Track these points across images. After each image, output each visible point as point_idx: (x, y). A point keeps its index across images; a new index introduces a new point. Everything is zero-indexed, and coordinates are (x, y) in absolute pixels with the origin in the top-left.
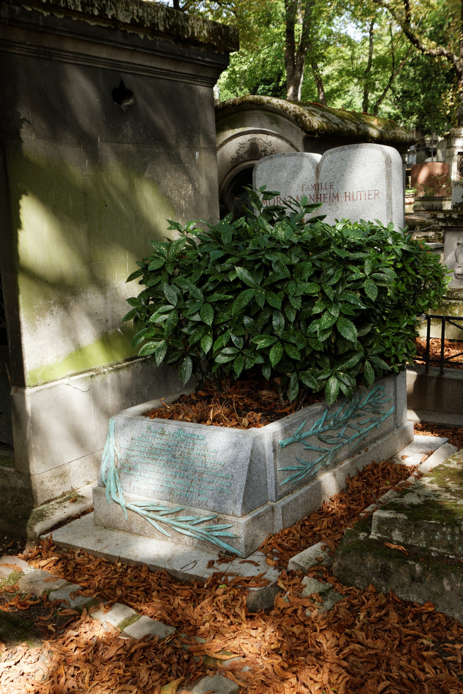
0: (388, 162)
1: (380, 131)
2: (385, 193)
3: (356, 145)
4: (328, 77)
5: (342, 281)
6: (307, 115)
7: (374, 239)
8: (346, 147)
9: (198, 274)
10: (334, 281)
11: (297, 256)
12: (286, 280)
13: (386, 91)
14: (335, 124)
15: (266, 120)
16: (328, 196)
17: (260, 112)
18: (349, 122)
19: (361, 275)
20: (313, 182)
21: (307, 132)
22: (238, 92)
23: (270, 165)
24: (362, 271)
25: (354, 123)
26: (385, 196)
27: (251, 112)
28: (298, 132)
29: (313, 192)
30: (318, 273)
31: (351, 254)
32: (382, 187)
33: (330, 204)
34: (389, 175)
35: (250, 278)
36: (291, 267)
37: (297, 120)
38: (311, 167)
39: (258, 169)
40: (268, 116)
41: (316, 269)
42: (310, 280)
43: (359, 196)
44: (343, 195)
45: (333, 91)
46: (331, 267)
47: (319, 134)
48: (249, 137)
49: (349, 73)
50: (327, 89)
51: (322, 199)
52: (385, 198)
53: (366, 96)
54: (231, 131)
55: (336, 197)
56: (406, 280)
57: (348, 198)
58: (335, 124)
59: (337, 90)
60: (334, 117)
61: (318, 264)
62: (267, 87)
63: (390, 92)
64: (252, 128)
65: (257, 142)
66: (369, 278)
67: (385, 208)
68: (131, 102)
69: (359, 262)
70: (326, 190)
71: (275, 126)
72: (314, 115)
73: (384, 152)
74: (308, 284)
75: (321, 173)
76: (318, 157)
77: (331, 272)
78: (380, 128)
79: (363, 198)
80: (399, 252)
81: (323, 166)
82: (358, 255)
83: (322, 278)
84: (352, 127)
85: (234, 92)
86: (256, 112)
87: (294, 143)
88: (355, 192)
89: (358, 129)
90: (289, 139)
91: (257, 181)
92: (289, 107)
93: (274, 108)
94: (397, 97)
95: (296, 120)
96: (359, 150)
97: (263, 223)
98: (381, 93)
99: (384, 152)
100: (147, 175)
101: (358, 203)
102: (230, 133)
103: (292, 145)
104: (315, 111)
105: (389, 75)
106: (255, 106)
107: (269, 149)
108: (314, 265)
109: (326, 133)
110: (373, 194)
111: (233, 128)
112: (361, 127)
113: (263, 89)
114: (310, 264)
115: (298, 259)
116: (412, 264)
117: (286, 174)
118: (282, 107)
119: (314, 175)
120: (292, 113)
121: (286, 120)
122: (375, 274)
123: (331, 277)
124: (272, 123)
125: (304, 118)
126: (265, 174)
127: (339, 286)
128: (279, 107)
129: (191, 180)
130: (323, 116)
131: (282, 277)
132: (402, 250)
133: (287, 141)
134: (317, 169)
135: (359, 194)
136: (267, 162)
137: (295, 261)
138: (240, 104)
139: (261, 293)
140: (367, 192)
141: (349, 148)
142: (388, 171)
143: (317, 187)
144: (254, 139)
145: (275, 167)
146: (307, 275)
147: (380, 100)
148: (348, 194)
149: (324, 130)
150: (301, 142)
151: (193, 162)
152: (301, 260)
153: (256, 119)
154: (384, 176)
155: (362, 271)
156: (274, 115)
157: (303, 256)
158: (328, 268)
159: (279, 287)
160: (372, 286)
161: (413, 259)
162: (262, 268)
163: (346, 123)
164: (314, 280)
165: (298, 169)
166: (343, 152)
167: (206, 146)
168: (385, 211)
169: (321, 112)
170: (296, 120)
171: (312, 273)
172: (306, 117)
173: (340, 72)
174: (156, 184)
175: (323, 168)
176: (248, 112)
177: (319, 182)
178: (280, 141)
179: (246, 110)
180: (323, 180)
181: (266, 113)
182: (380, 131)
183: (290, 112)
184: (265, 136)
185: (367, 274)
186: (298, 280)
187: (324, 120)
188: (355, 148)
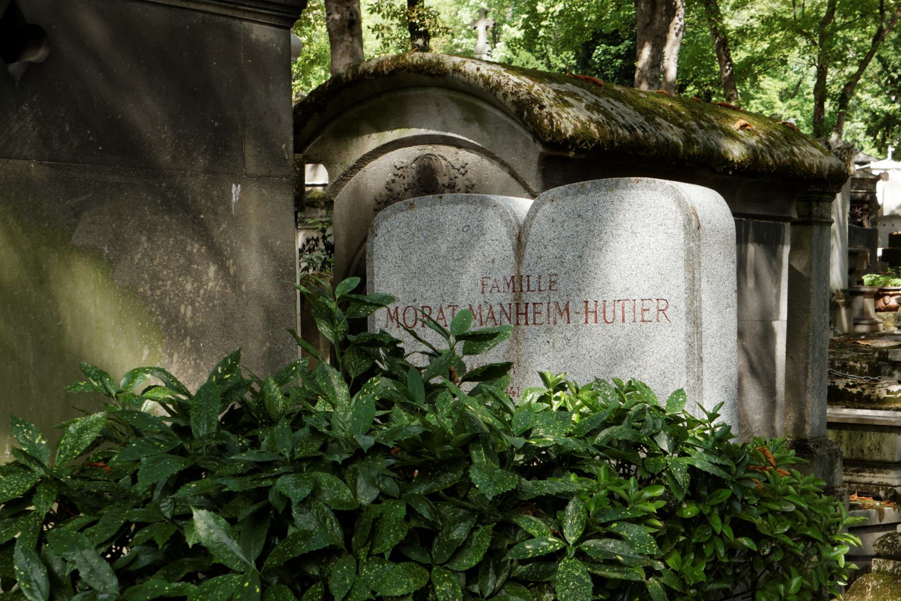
0: (693, 227)
1: (749, 147)
2: (683, 307)
3: (612, 180)
4: (741, 32)
5: (493, 556)
6: (546, 103)
7: (628, 432)
8: (588, 184)
9: (112, 519)
10: (469, 560)
11: (372, 483)
12: (330, 553)
13: (863, 65)
14: (624, 126)
15: (455, 113)
16: (544, 309)
17: (439, 93)
18: (665, 123)
19: (551, 543)
20: (509, 272)
21: (545, 144)
22: (552, 57)
23: (408, 225)
24: (559, 534)
25: (680, 126)
26: (682, 316)
27: (420, 92)
28: (526, 144)
29: (506, 297)
30: (424, 536)
31: (527, 484)
32: (675, 289)
33: (548, 330)
34: (692, 262)
35: (234, 546)
36: (348, 517)
37: (523, 111)
38: (504, 230)
39: (380, 232)
40: (459, 103)
41: (414, 523)
42: (398, 556)
43: (619, 313)
44: (581, 307)
45: (749, 63)
46: (463, 519)
47: (579, 151)
48: (414, 151)
49: (785, 24)
50: (739, 56)
51: (530, 316)
52: (683, 322)
53: (821, 75)
54: (374, 135)
55: (565, 311)
56: (708, 551)
57: (591, 317)
58: (624, 126)
59: (761, 60)
60: (629, 110)
61: (424, 510)
62: (613, 49)
63: (874, 66)
64: (423, 132)
65: (435, 164)
66: (571, 552)
67: (683, 346)
68: (38, 55)
69: (552, 506)
70: (542, 290)
71: (475, 128)
72: (567, 104)
73: (680, 203)
74: (388, 566)
75: (529, 250)
76: (523, 205)
77: (459, 533)
78: (753, 141)
79: (629, 317)
80: (682, 477)
81: (533, 231)
82: (550, 486)
83: (435, 549)
84: (674, 135)
85: (543, 57)
86: (431, 91)
87: (520, 169)
88: (610, 300)
89: (689, 141)
90: (506, 160)
91: (376, 263)
92: (504, 81)
93: (468, 84)
94: (892, 78)
95: (520, 114)
96: (618, 192)
97: (329, 381)
98: (854, 69)
99: (680, 203)
100: (79, 238)
101: (616, 329)
102: (373, 141)
103: (514, 175)
104: (573, 95)
105: (872, 29)
106: (427, 79)
107: (460, 182)
108: (411, 513)
109: (598, 147)
110: (654, 310)
111: (379, 129)
112: (700, 136)
113: (605, 52)
114: (400, 510)
115: (375, 493)
116: (725, 510)
117: (444, 247)
118: (487, 81)
119: (510, 252)
120: (510, 98)
121: (499, 114)
122: (591, 543)
123: (460, 549)
124: (467, 120)
125: (536, 109)
126: (394, 245)
127: (486, 572)
128: (481, 83)
129: (217, 254)
130: (593, 107)
131: (319, 543)
132: (692, 469)
133: (503, 164)
134: (519, 239)
135: (618, 306)
136: (400, 215)
137: (365, 498)
138: (392, 73)
139: (251, 589)
140: (638, 302)
141: (597, 189)
142: (689, 251)
143: (518, 283)
144: (429, 156)
145: (419, 230)
146: (389, 541)
147: (852, 84)
148: (591, 306)
149: (592, 140)
150: (534, 167)
151: (221, 209)
152: (384, 496)
153: (433, 110)
154: (681, 263)
155: (559, 534)
156: (470, 100)
157: (389, 485)
158: (455, 522)
159: (314, 571)
160: (579, 579)
161: (725, 494)
162: (265, 519)
163: (658, 126)
164: (414, 555)
165: (473, 234)
166: (580, 198)
167: (263, 171)
168: (682, 355)
169: (591, 98)
170: (520, 114)
171: (402, 536)
172: (542, 107)
173: (767, 22)
174: (109, 261)
175: (532, 237)
176: (411, 92)
177: (523, 272)
178: (486, 162)
179: (407, 88)
180: (533, 267)
181: (454, 95)
182: (749, 147)
183: (505, 95)
184: (453, 150)
185: (572, 539)
186: (362, 554)
187: (596, 116)
188: (611, 189)
